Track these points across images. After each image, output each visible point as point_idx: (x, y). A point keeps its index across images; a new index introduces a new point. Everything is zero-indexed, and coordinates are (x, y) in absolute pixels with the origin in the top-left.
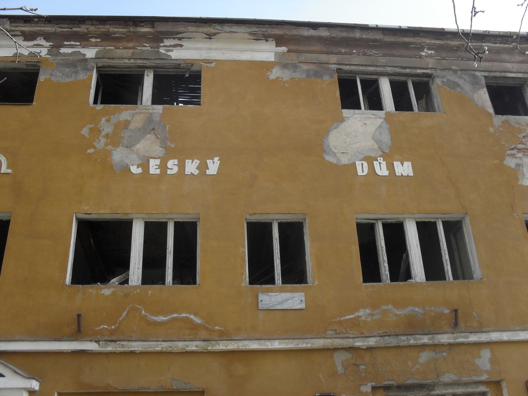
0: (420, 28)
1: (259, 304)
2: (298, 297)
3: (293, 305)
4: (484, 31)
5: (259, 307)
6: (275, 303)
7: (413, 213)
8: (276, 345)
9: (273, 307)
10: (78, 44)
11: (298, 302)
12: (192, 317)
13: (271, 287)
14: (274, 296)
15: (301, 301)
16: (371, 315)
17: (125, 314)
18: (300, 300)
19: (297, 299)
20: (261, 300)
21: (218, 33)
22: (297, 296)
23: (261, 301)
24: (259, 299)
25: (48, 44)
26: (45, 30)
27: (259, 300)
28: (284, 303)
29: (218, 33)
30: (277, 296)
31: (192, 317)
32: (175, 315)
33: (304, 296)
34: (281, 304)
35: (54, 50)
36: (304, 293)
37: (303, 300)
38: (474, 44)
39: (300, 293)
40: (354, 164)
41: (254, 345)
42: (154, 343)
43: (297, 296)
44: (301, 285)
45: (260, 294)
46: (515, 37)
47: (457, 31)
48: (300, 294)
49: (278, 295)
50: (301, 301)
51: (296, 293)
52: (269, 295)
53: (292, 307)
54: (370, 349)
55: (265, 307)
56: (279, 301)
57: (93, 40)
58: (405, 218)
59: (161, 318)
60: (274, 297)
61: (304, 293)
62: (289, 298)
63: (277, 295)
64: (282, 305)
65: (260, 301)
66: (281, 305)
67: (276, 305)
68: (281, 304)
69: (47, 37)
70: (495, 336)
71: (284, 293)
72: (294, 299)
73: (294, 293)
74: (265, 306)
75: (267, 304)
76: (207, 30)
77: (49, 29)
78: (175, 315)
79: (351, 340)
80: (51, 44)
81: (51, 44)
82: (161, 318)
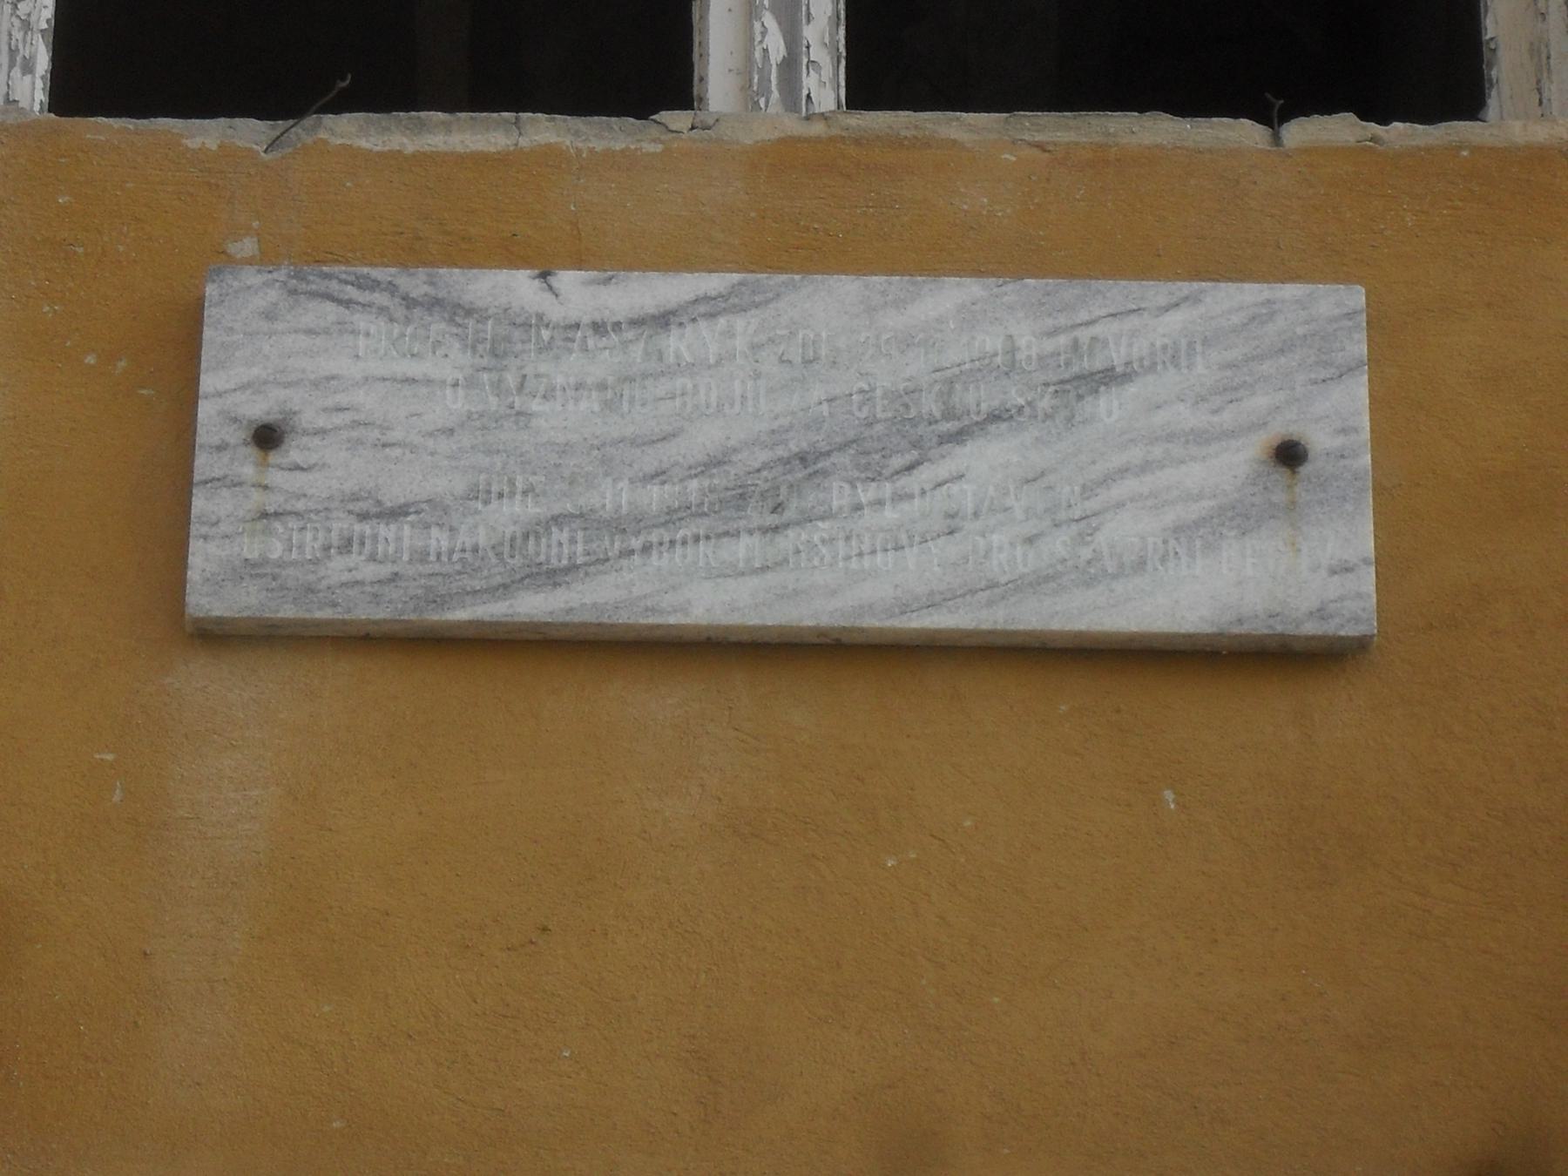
1: (199, 503)
2: (1203, 371)
3: (1058, 544)
5: (203, 558)
6: (612, 496)
7: (387, 383)
9: (553, 577)
11: (1193, 475)
13: (549, 157)
14: (598, 328)
15: (1289, 455)
18: (1257, 446)
19: (1186, 417)
20: (258, 409)
22: (1174, 356)
23: (267, 437)
24: (208, 382)
27: (206, 410)
28: (839, 495)
30: (676, 343)
33: (1359, 347)
34: (757, 516)
36: (1356, 297)
37: (1319, 440)
39: (1251, 293)
43: (1174, 356)
44: (1302, 132)
45: (251, 277)
46: (895, 528)
47: (1480, 116)
48: (1269, 312)
49: (710, 308)
50: (1289, 455)
51: (1157, 292)
52: (457, 311)
53: (1040, 582)
55: (337, 568)
56: (705, 438)
60: (603, 362)
61: (1356, 297)
62: (978, 398)
63: (663, 320)
64: (788, 541)
65: (236, 436)
66: (743, 548)
67: (617, 526)
68: (757, 516)
71: (847, 287)
72: (1109, 407)
73: (1119, 292)
74: (346, 546)
75: (397, 513)
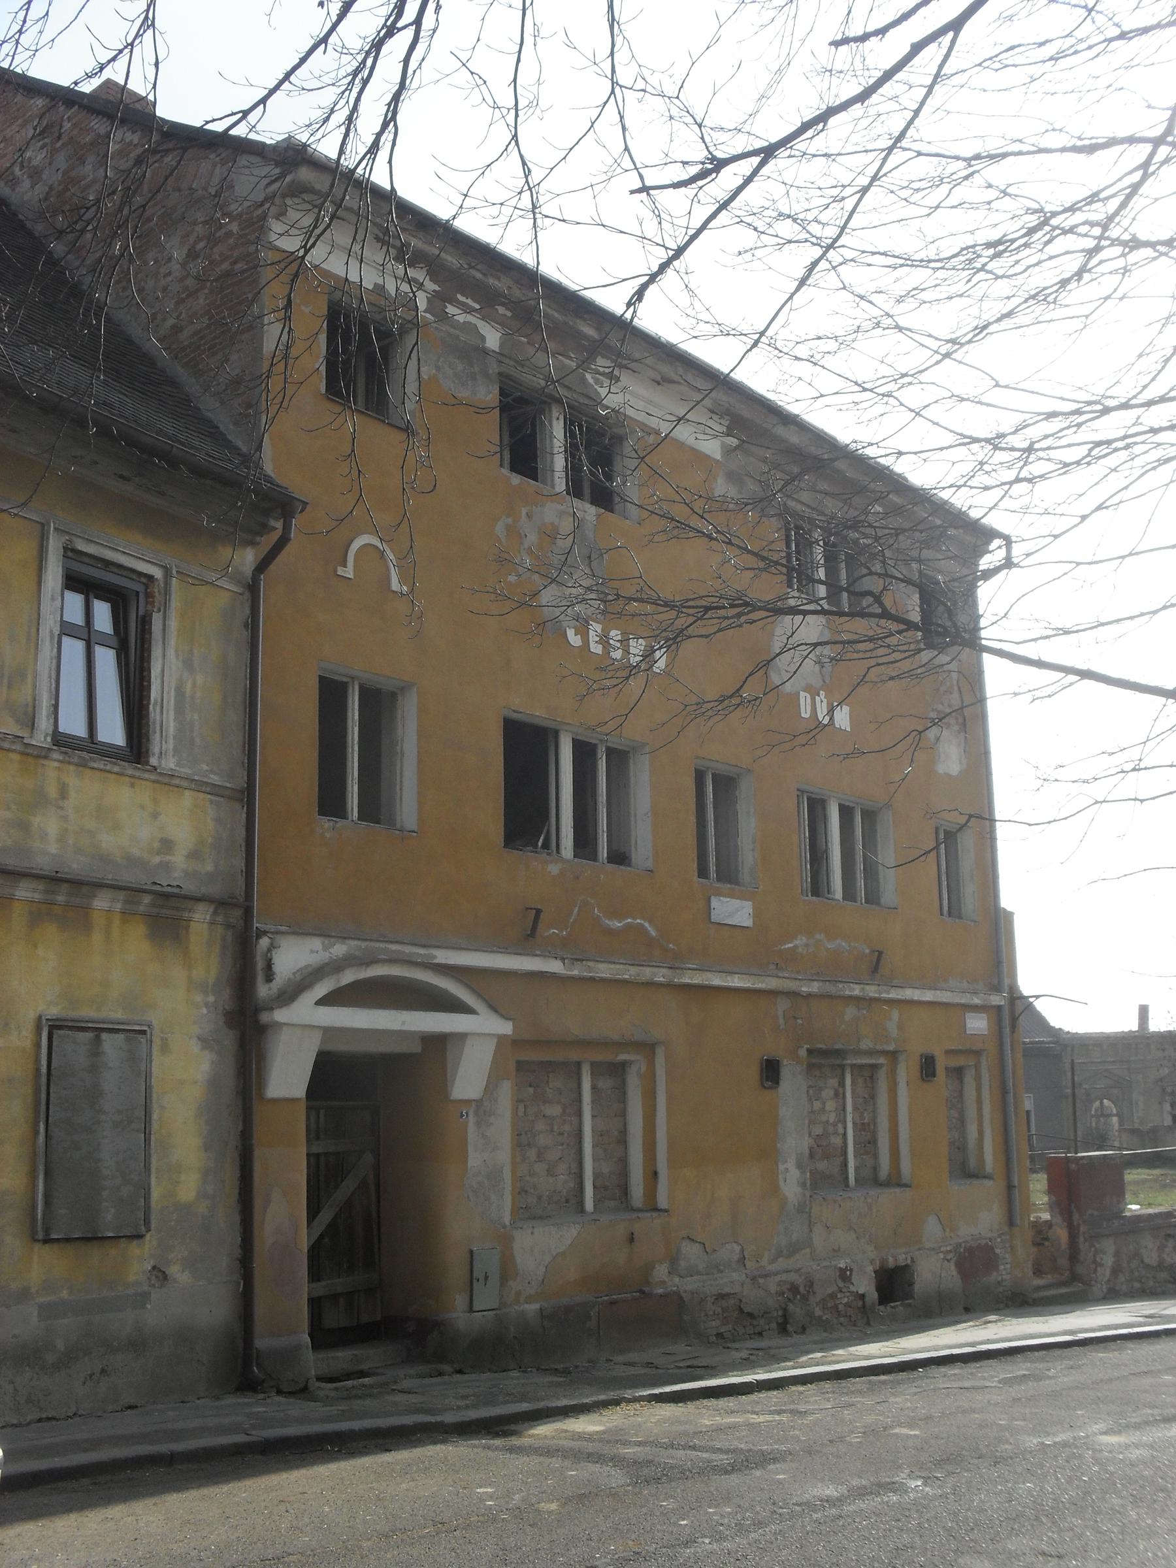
0: (822, 431)
4: (668, 342)
8: (736, 982)
10: (478, 307)
12: (646, 925)
16: (807, 945)
17: (576, 910)
21: (679, 383)
25: (431, 286)
26: (446, 260)
29: (679, 383)
31: (646, 925)
32: (629, 920)
35: (438, 300)
38: (549, 311)
40: (798, 694)
41: (717, 981)
42: (622, 966)
54: (810, 995)
57: (501, 310)
58: (830, 797)
59: (617, 924)
69: (435, 269)
70: (909, 994)
76: (957, 533)
77: (451, 259)
78: (629, 920)
79: (798, 983)
80: (437, 288)
81: (437, 288)
82: (617, 924)
